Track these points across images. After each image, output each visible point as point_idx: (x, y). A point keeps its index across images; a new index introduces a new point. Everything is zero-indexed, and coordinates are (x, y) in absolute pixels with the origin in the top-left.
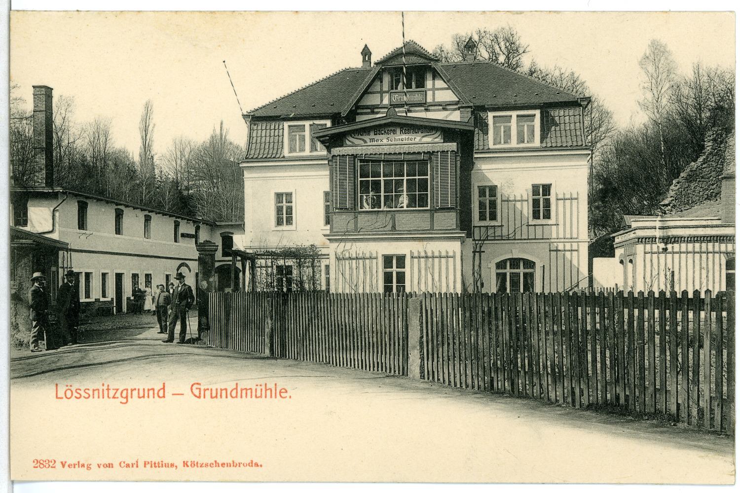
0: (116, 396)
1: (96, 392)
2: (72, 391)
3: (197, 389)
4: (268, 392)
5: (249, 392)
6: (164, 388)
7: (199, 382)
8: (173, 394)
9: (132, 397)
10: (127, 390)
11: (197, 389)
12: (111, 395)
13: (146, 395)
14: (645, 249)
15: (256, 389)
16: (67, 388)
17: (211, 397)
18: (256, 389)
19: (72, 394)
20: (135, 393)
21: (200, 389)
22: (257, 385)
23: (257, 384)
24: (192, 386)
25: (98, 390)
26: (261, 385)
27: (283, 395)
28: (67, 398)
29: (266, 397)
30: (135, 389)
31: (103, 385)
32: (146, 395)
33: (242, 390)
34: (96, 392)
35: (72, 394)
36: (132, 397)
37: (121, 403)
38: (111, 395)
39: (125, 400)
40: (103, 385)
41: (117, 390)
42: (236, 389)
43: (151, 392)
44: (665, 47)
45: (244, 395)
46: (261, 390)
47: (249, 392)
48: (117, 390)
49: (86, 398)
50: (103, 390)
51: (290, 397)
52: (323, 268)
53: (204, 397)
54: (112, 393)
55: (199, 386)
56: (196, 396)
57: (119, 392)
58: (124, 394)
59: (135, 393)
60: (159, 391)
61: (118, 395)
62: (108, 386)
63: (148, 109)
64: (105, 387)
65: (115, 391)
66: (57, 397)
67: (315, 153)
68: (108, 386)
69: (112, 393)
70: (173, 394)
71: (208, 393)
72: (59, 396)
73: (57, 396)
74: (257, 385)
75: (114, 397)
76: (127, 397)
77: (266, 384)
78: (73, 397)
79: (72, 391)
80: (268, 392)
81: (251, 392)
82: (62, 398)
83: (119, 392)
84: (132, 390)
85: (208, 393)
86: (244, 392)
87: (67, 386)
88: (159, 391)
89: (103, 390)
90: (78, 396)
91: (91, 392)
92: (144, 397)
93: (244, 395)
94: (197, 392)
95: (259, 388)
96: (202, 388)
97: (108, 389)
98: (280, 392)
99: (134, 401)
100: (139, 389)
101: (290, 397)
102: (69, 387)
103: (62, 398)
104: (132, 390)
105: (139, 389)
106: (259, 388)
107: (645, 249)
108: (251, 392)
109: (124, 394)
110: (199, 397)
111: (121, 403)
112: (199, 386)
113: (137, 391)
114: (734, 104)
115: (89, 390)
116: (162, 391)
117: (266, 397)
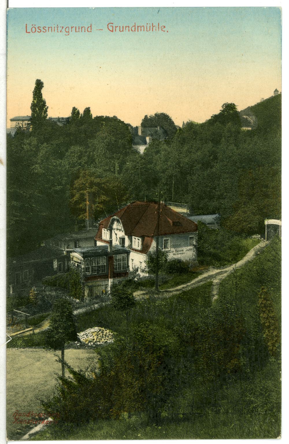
0: (134, 27)
2: (35, 28)
3: (111, 26)
5: (142, 28)
6: (91, 26)
8: (159, 23)
11: (111, 26)
13: (124, 28)
14: (136, 251)
19: (36, 30)
22: (147, 24)
23: (148, 23)
28: (33, 32)
32: (124, 28)
33: (138, 27)
35: (36, 30)
45: (139, 30)
47: (142, 28)
48: (63, 27)
49: (39, 32)
52: (140, 246)
53: (116, 31)
54: (60, 29)
56: (111, 31)
57: (64, 28)
60: (88, 27)
63: (39, 85)
64: (56, 26)
71: (118, 29)
72: (28, 31)
73: (26, 31)
74: (147, 24)
76: (69, 32)
77: (153, 24)
78: (37, 31)
79: (35, 28)
83: (64, 28)
84: (116, 27)
86: (139, 28)
88: (88, 27)
90: (39, 31)
91: (47, 29)
94: (111, 29)
95: (148, 26)
96: (114, 25)
102: (33, 26)
105: (76, 27)
106: (148, 26)
107: (136, 251)
110: (112, 31)
112: (111, 25)
113: (119, 27)
114: (35, 89)
115: (40, 27)
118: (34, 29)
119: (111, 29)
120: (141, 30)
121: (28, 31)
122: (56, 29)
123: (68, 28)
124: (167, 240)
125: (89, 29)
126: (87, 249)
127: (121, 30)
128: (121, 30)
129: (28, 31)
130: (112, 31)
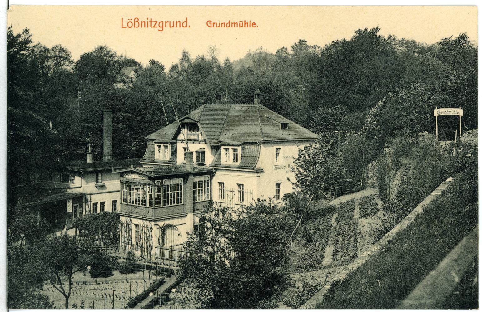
1: (143, 23)
4: (246, 25)
6: (186, 21)
7: (185, 222)
8: (122, 19)
9: (166, 27)
10: (163, 22)
12: (153, 26)
13: (175, 25)
15: (240, 23)
16: (129, 21)
17: (217, 27)
18: (240, 23)
20: (168, 24)
21: (211, 23)
24: (207, 25)
25: (145, 22)
26: (242, 21)
27: (254, 26)
29: (148, 27)
30: (168, 22)
31: (148, 19)
32: (175, 25)
33: (232, 23)
34: (143, 23)
36: (166, 27)
37: (159, 30)
38: (153, 26)
39: (161, 29)
40: (148, 19)
41: (156, 22)
42: (229, 23)
43: (178, 24)
44: (173, 66)
46: (242, 23)
48: (156, 22)
50: (148, 22)
51: (258, 26)
54: (153, 24)
55: (210, 22)
58: (161, 25)
59: (168, 24)
61: (157, 25)
62: (151, 19)
65: (155, 23)
66: (122, 27)
67: (178, 204)
68: (151, 19)
69: (153, 24)
70: (122, 19)
72: (179, 23)
75: (154, 27)
76: (163, 27)
80: (246, 25)
81: (237, 25)
82: (126, 27)
84: (166, 22)
85: (215, 25)
87: (129, 19)
89: (148, 22)
92: (173, 27)
93: (223, 26)
94: (210, 25)
95: (241, 23)
97: (151, 22)
98: (252, 24)
99: (167, 29)
100: (217, 23)
101: (258, 26)
102: (130, 20)
103: (126, 27)
104: (166, 22)
105: (170, 22)
106: (241, 23)
108: (237, 25)
109: (161, 25)
110: (211, 27)
111: (159, 30)
112: (210, 22)
113: (216, 24)
116: (185, 23)
117: (148, 27)
118: (130, 25)
119: (210, 25)
120: (235, 26)
121: (123, 26)
122: (149, 24)
123: (162, 23)
124: (280, 149)
125: (228, 25)
126: (155, 168)
127: (172, 25)
128: (172, 25)
129: (123, 26)
130: (211, 27)
